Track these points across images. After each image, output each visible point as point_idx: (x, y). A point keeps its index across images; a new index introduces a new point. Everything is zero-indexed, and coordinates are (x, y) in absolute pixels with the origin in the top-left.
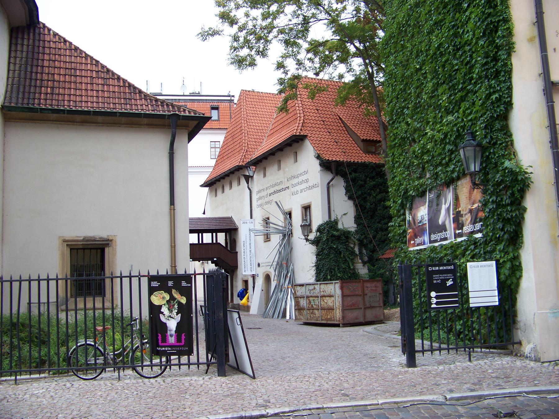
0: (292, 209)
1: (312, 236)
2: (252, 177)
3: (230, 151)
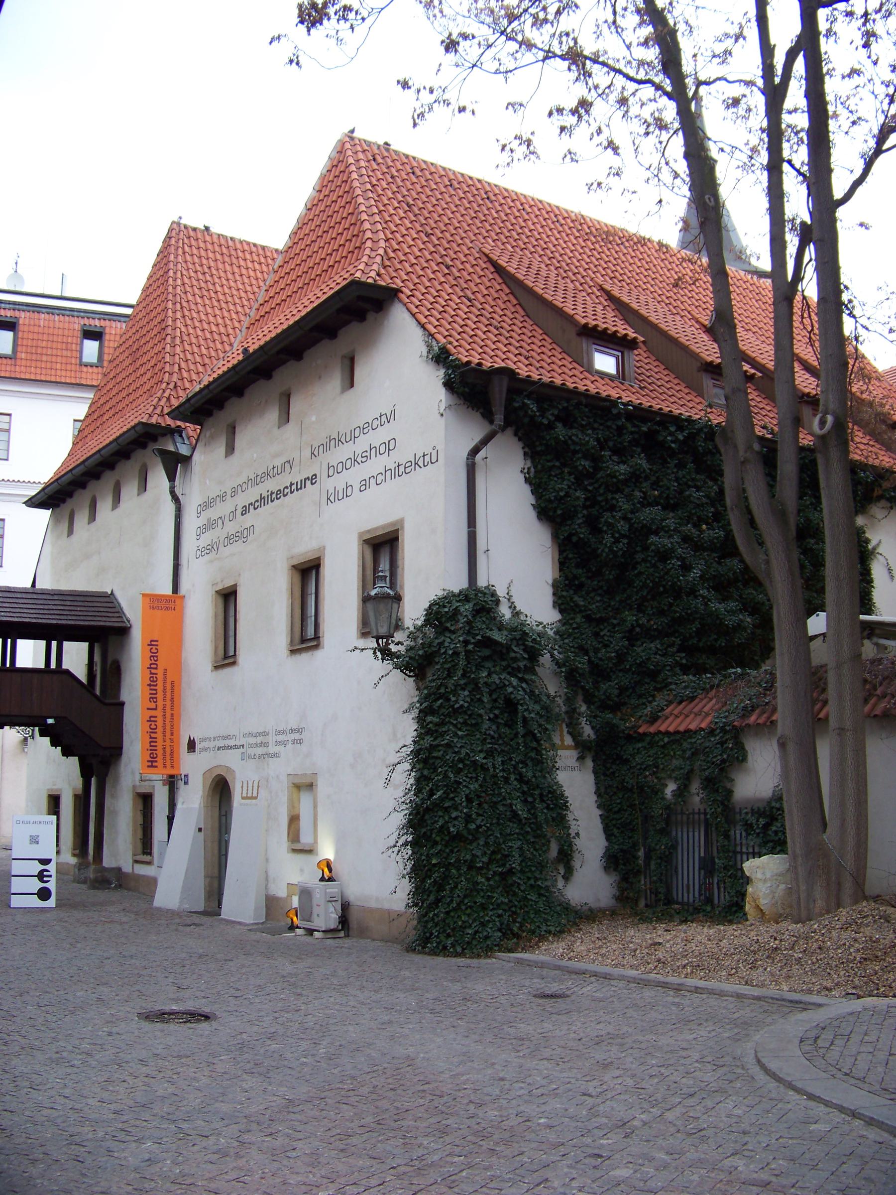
0: (323, 549)
1: (400, 643)
2: (186, 460)
3: (124, 394)
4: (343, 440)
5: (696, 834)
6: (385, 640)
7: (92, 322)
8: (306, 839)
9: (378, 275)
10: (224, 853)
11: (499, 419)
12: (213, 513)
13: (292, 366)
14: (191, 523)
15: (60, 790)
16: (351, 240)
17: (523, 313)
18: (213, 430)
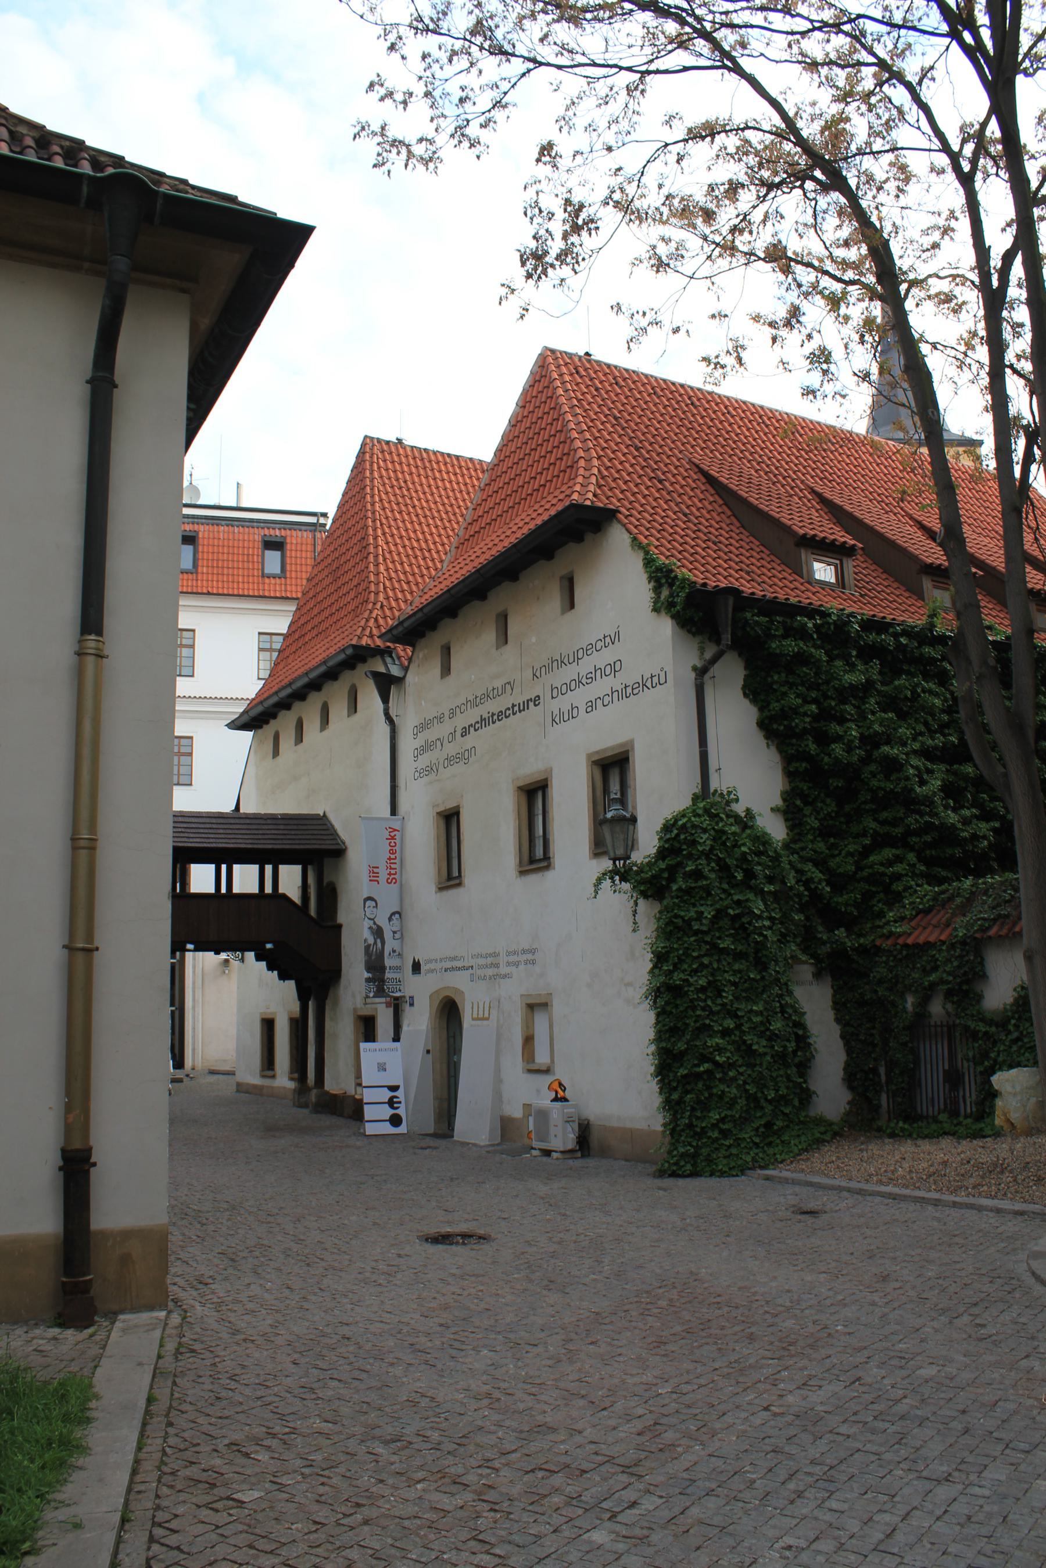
0: (550, 771)
2: (399, 681)
3: (327, 613)
4: (566, 661)
5: (940, 1046)
6: (622, 862)
7: (272, 532)
8: (542, 1058)
9: (595, 495)
10: (452, 1074)
11: (727, 638)
12: (431, 735)
13: (507, 587)
14: (407, 744)
15: (275, 1013)
16: (562, 459)
17: (738, 525)
18: (426, 651)
